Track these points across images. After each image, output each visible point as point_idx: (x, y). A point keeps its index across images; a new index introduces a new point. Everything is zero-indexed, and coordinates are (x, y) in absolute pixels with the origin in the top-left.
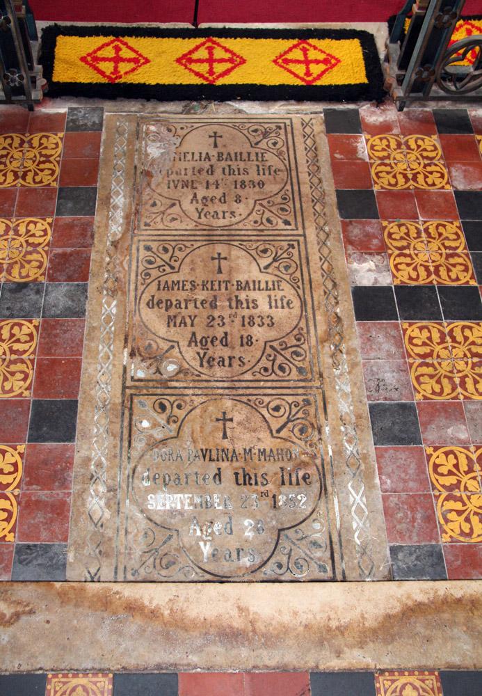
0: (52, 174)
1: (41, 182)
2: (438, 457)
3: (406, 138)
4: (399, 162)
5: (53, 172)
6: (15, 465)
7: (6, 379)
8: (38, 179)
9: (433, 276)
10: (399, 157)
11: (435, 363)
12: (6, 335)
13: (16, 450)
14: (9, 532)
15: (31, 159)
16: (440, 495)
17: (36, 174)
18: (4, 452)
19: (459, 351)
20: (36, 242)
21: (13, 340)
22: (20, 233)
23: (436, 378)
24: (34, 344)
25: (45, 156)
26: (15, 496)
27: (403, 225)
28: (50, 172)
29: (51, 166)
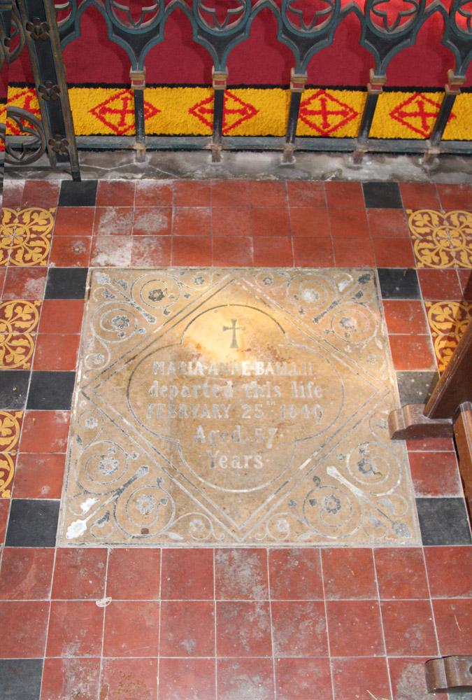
0: (42, 253)
1: (12, 363)
2: (416, 216)
3: (449, 214)
4: (442, 239)
5: (27, 349)
6: (13, 429)
7: (7, 353)
8: (28, 257)
9: (455, 261)
10: (441, 234)
11: (435, 240)
12: (9, 313)
13: (33, 303)
14: (6, 489)
15: (21, 236)
16: (437, 336)
17: (26, 252)
18: (2, 417)
19: (455, 233)
20: (40, 230)
21: (15, 318)
22: (6, 316)
23: (435, 252)
24: (15, 439)
25: (36, 233)
26: (48, 239)
27: (447, 306)
28: (41, 250)
29: (25, 343)
